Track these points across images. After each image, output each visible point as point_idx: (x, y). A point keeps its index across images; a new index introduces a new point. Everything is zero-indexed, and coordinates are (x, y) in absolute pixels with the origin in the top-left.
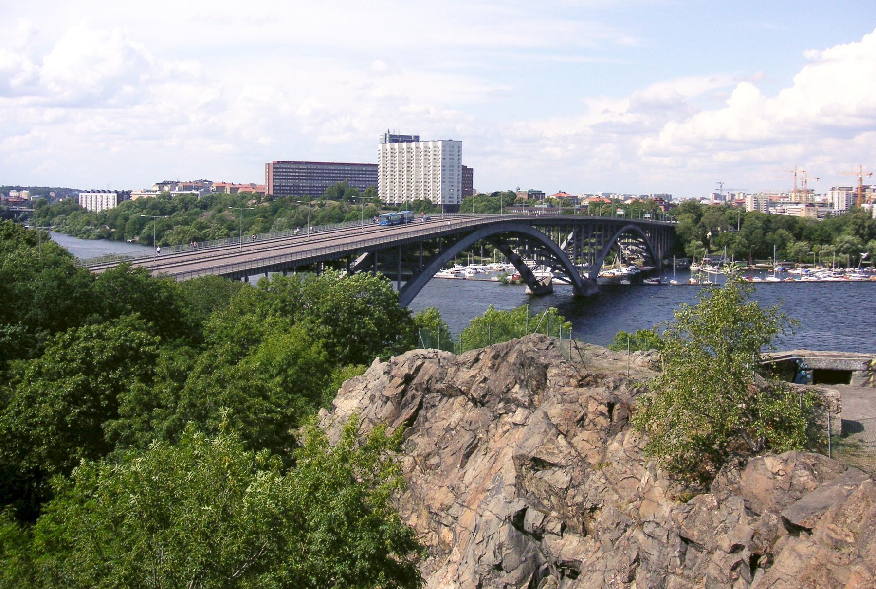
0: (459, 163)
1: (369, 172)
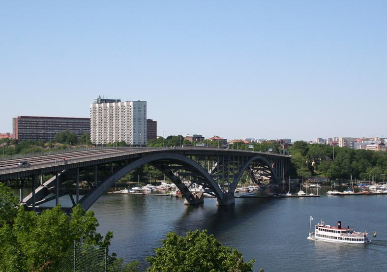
0: (145, 119)
1: (85, 123)
